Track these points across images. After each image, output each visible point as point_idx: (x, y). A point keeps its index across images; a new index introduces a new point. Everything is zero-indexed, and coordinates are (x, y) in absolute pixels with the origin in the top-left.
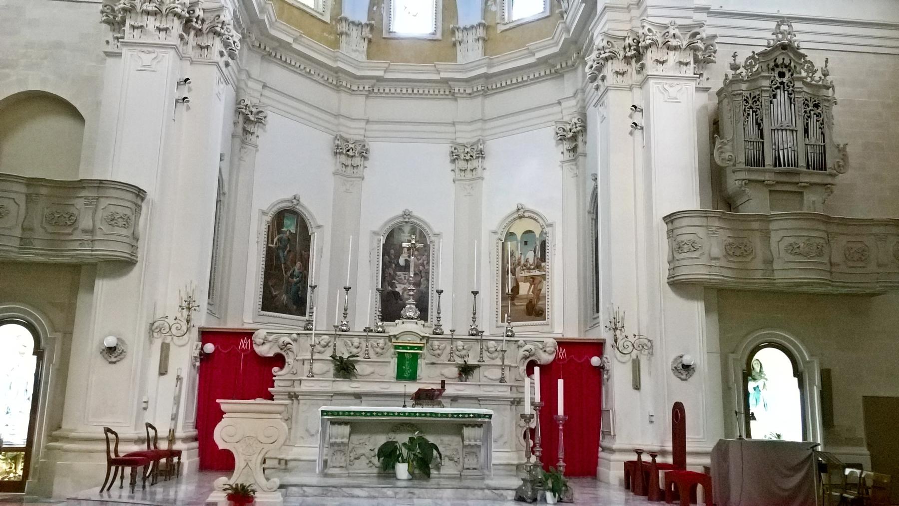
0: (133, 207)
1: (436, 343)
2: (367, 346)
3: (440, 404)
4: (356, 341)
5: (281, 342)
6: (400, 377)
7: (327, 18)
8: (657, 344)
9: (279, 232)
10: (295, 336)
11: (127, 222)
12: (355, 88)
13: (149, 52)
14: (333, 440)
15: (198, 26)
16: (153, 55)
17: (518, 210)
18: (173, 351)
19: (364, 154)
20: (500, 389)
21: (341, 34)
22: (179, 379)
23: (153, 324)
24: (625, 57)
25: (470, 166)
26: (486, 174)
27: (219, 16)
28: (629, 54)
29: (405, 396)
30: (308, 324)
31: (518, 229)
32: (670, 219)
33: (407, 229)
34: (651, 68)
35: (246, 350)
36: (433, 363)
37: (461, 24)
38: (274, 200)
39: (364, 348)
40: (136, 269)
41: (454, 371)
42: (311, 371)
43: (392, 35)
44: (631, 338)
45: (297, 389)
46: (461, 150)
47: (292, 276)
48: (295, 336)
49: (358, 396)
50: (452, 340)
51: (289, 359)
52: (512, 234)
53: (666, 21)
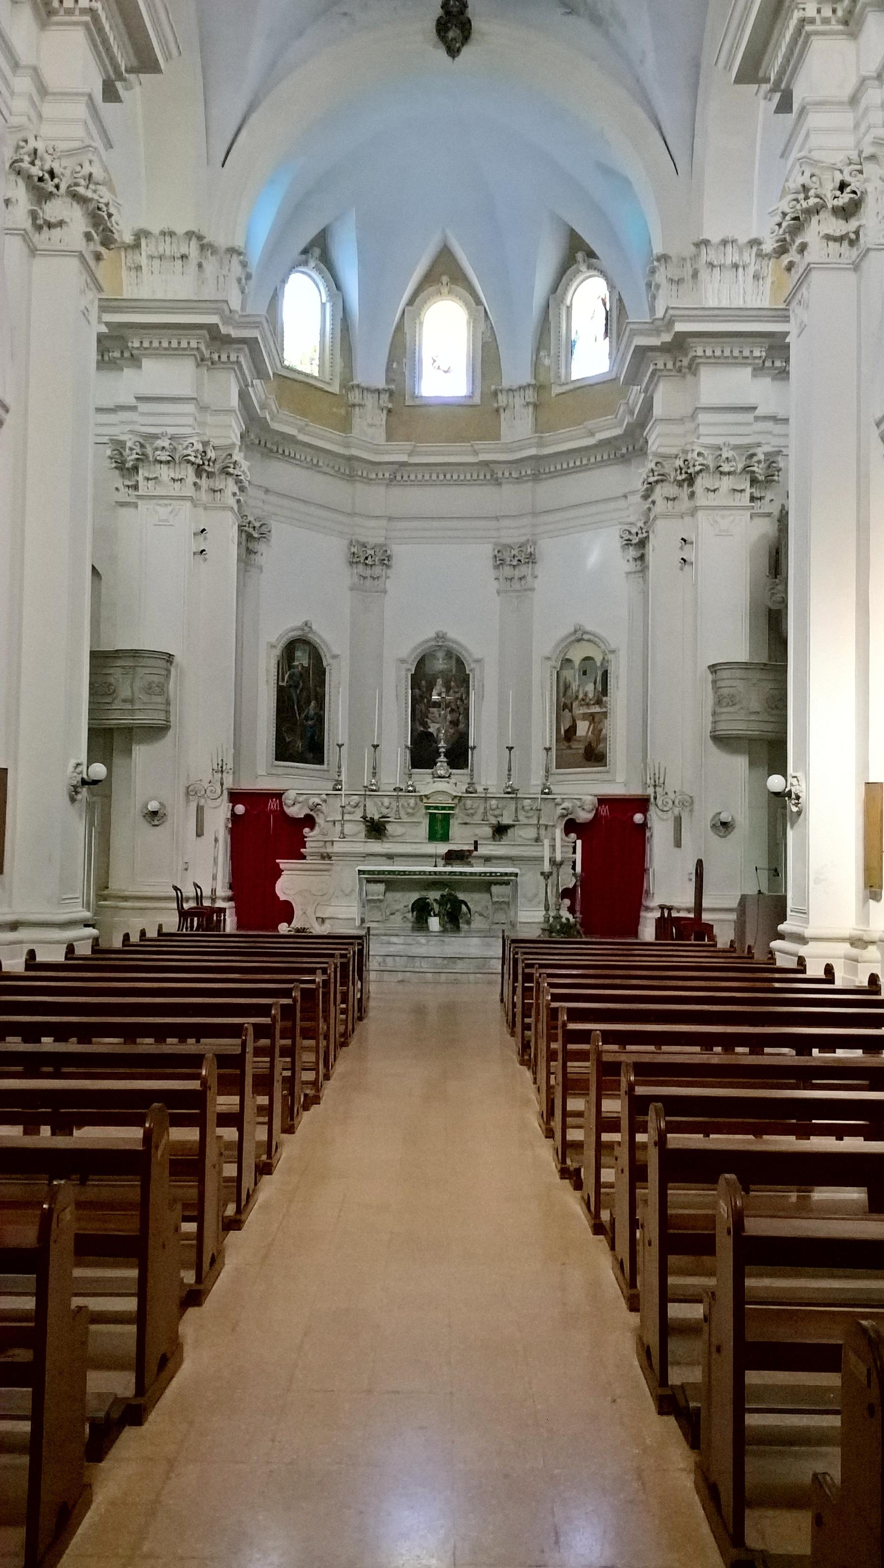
0: (164, 673)
1: (469, 803)
2: (398, 807)
3: (470, 865)
4: (386, 801)
5: (311, 803)
6: (433, 837)
7: (335, 389)
8: (696, 800)
9: (290, 667)
10: (324, 797)
11: (162, 689)
12: (373, 476)
13: (166, 505)
14: (370, 897)
15: (210, 470)
16: (170, 508)
17: (576, 631)
18: (208, 815)
19: (386, 561)
20: (534, 848)
21: (354, 406)
22: (216, 840)
23: (188, 788)
24: (675, 480)
25: (517, 573)
26: (537, 584)
27: (230, 455)
28: (680, 478)
29: (436, 856)
30: (336, 785)
31: (577, 655)
32: (714, 668)
33: (440, 655)
34: (702, 499)
35: (275, 811)
36: (466, 824)
37: (506, 384)
38: (280, 632)
39: (395, 808)
40: (170, 733)
41: (488, 831)
42: (342, 832)
43: (418, 402)
44: (672, 795)
45: (329, 850)
46: (507, 556)
47: (307, 718)
48: (324, 797)
49: (390, 857)
50: (486, 799)
51: (320, 820)
52: (569, 661)
53: (719, 441)
